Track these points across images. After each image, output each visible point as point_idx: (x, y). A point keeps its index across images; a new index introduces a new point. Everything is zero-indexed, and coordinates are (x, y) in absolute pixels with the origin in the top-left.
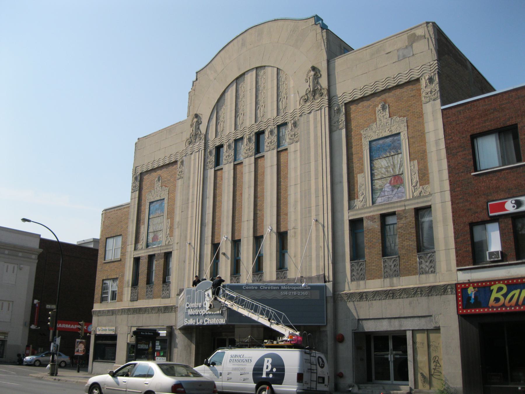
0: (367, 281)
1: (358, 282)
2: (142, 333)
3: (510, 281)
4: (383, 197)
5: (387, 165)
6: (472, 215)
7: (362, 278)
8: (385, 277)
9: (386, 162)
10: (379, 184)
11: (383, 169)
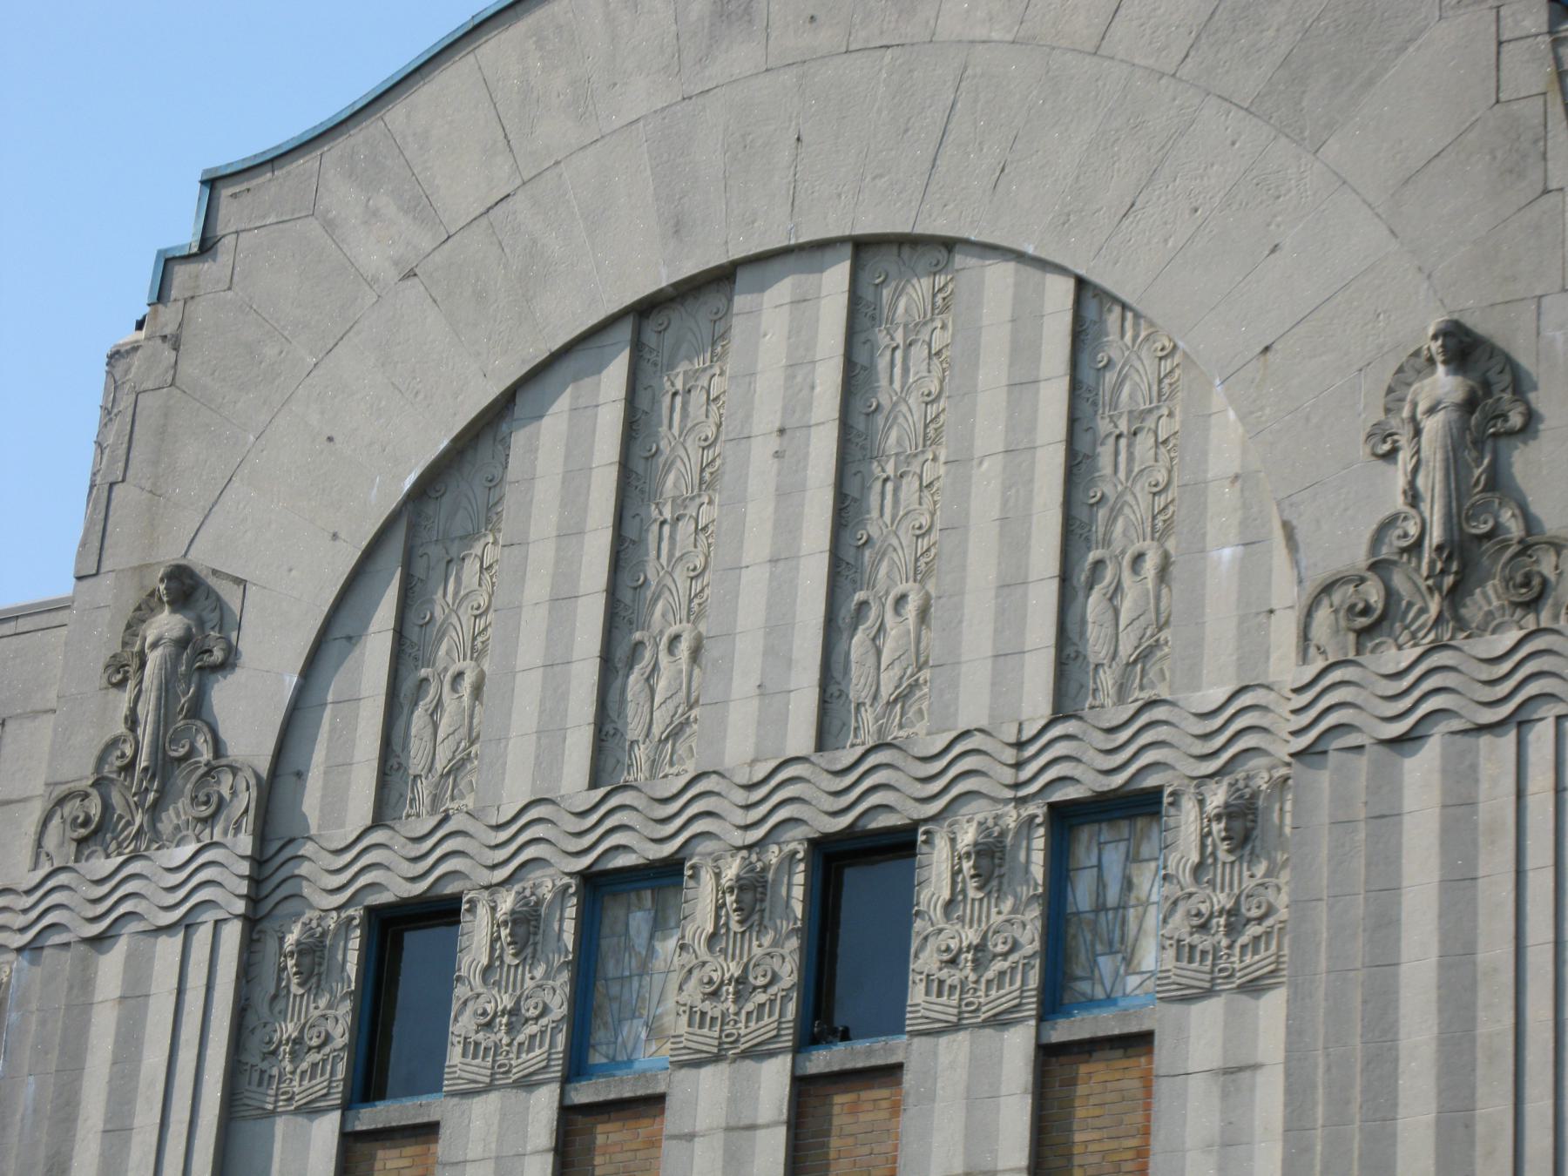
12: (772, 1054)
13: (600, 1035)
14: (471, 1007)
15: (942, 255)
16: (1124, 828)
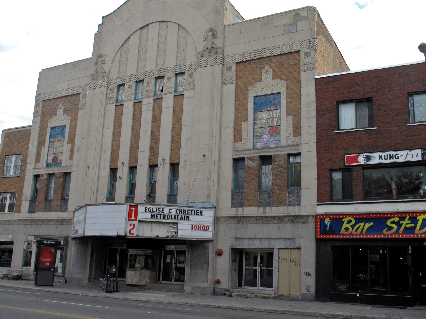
0: (245, 208)
1: (237, 208)
2: (45, 242)
3: (334, 217)
4: (262, 142)
5: (267, 117)
6: (332, 164)
7: (241, 205)
8: (259, 206)
9: (266, 114)
10: (259, 132)
11: (264, 120)
12: (172, 93)
13: (137, 96)
14: (303, 62)
15: (167, 22)
16: (182, 75)
